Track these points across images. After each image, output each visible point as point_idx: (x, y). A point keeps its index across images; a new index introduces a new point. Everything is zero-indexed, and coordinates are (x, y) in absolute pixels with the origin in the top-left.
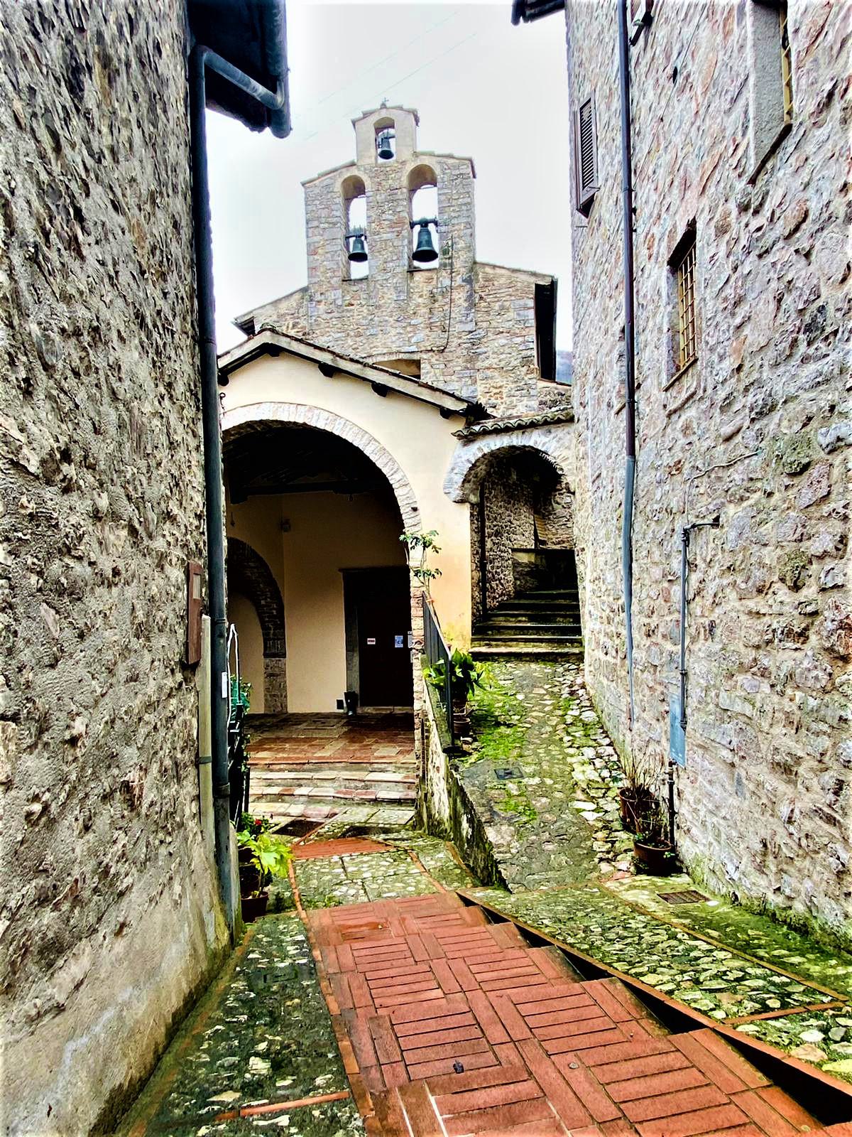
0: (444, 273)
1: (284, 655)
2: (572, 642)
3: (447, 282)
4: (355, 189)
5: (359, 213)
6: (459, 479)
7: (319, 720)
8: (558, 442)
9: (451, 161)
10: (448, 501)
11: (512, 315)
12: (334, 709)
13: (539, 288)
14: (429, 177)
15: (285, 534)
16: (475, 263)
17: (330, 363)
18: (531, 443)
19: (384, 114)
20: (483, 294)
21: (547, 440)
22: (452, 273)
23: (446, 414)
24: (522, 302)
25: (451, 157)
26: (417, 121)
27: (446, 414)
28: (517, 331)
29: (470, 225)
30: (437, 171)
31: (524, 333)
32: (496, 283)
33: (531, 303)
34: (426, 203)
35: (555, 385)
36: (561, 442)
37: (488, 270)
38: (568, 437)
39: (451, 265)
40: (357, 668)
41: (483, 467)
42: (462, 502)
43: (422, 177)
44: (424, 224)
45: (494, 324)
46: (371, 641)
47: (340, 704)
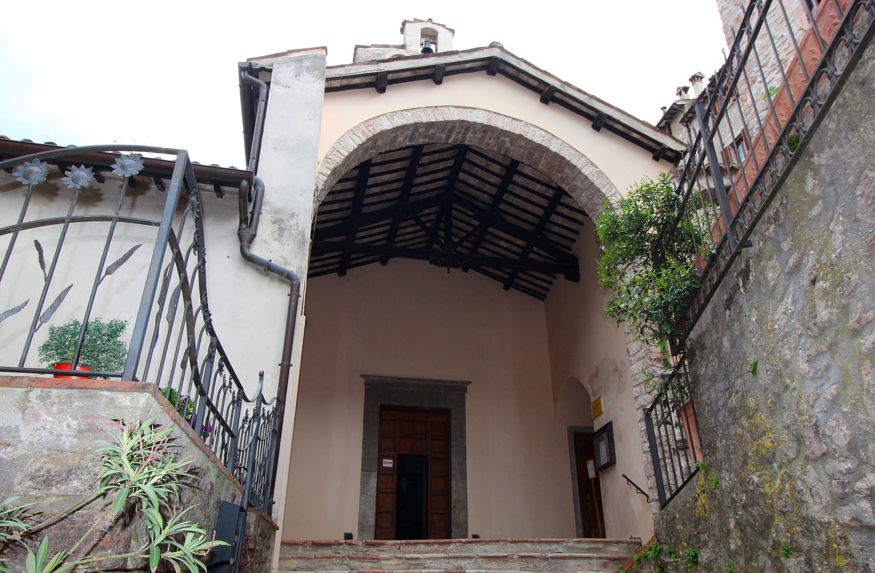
46: (388, 463)
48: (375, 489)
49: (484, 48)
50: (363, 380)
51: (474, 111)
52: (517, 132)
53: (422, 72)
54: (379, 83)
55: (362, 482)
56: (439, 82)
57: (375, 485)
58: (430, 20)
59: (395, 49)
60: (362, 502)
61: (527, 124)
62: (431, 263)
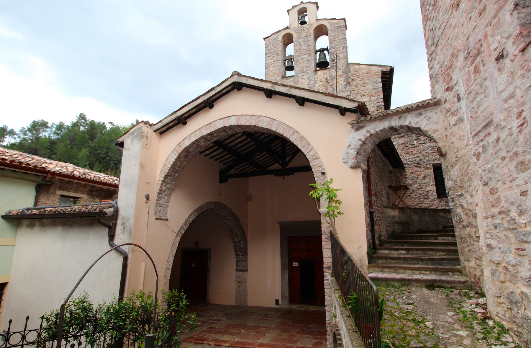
0: (333, 70)
1: (247, 271)
2: (453, 271)
3: (335, 74)
4: (288, 39)
5: (290, 50)
6: (353, 153)
7: (264, 313)
8: (428, 120)
9: (334, 21)
10: (347, 168)
11: (369, 86)
12: (274, 305)
13: (384, 73)
14: (324, 30)
15: (249, 203)
16: (348, 64)
17: (270, 88)
18: (407, 123)
19: (302, 6)
20: (353, 78)
22: (336, 70)
23: (343, 111)
24: (375, 80)
26: (318, 7)
27: (343, 111)
28: (373, 94)
29: (346, 48)
30: (328, 26)
31: (377, 94)
32: (360, 72)
33: (380, 80)
34: (323, 42)
36: (431, 120)
37: (356, 66)
38: (436, 116)
39: (336, 66)
40: (287, 280)
41: (370, 145)
42: (355, 167)
43: (320, 31)
44: (322, 51)
45: (360, 91)
46: (295, 264)
47: (277, 302)
48: (287, 279)
49: (228, 78)
50: (279, 225)
51: (231, 118)
52: (253, 124)
53: (201, 106)
54: (181, 120)
55: (282, 275)
56: (185, 123)
57: (287, 277)
58: (302, 2)
59: (283, 31)
60: (282, 285)
61: (259, 117)
62: (275, 175)
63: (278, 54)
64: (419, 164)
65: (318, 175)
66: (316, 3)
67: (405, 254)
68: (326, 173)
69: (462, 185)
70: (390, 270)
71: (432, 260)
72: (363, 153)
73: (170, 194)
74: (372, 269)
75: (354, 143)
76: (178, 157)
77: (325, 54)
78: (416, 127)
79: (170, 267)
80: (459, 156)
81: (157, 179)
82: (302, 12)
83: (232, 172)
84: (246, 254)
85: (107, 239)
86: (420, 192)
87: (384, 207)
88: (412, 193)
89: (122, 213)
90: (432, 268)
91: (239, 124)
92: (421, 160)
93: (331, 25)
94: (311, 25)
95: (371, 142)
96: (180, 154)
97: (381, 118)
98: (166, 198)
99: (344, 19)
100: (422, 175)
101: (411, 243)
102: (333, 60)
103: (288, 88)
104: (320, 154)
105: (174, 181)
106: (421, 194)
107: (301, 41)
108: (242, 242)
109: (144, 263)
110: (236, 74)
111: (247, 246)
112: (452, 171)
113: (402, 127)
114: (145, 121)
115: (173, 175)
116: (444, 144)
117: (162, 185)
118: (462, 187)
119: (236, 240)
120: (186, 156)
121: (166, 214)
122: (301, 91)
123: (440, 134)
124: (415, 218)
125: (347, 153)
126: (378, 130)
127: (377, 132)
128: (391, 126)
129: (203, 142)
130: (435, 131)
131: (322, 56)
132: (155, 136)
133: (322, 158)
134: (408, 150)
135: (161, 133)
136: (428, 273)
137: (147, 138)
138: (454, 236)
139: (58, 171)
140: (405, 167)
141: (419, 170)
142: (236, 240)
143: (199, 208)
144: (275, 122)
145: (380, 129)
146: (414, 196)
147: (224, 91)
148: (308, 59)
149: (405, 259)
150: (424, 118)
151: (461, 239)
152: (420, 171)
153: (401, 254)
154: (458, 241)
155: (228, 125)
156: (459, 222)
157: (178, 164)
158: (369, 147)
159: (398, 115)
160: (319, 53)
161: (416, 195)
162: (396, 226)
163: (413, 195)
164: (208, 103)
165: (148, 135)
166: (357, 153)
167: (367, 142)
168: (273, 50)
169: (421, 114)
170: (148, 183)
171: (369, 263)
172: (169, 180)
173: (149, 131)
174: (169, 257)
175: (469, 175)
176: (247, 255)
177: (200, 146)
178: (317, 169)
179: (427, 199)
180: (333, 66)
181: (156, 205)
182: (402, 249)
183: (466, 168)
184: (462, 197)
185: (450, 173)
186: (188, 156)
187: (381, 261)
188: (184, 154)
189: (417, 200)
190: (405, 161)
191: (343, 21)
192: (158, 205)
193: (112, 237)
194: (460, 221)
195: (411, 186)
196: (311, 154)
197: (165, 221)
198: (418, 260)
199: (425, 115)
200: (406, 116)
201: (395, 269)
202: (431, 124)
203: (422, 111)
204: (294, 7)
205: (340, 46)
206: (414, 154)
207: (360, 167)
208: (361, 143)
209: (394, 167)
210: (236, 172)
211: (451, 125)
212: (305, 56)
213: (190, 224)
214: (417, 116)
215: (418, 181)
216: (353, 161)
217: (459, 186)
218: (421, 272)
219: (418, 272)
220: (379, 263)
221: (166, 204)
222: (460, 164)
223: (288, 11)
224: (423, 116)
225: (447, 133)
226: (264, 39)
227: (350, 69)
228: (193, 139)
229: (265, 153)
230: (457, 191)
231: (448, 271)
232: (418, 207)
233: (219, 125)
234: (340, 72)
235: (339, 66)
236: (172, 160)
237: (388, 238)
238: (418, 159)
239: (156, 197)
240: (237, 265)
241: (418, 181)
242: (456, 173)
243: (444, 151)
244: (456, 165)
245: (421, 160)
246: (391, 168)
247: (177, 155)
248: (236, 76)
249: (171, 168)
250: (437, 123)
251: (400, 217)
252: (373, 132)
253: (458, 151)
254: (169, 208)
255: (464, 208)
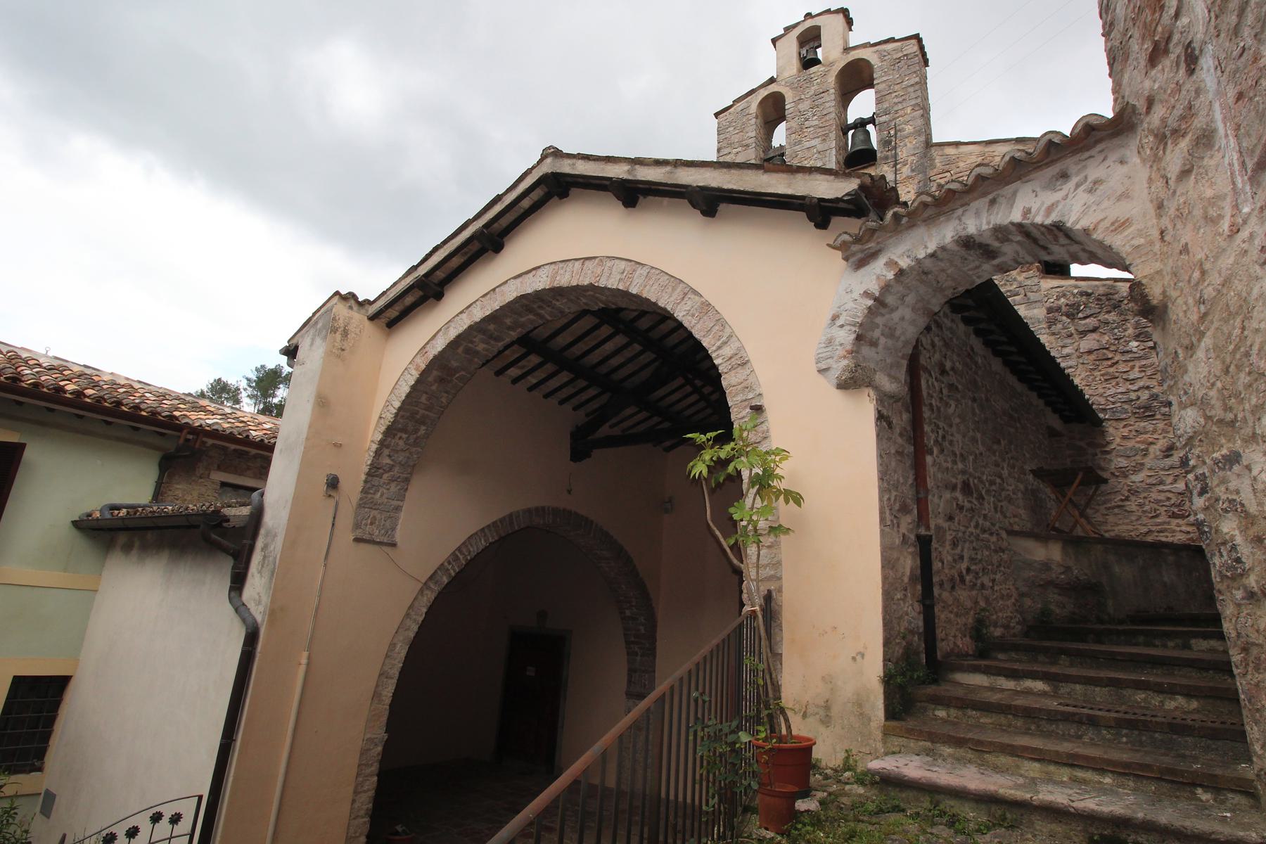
2: (1217, 786)
6: (845, 337)
8: (1090, 191)
10: (827, 387)
17: (625, 176)
18: (1016, 216)
19: (810, 23)
21: (1058, 196)
22: (895, 166)
25: (892, 40)
26: (850, 22)
32: (961, 164)
35: (1072, 282)
37: (950, 151)
38: (1123, 170)
42: (849, 384)
43: (856, 77)
44: (861, 124)
49: (533, 168)
58: (808, 16)
63: (747, 146)
64: (1147, 408)
65: (744, 413)
66: (844, 12)
67: (1044, 694)
68: (766, 406)
69: (1230, 416)
70: (961, 752)
71: (1134, 725)
72: (883, 340)
73: (407, 480)
74: (897, 741)
75: (850, 305)
76: (418, 381)
77: (868, 133)
78: (1048, 222)
79: (395, 672)
80: (1209, 292)
81: (369, 438)
82: (810, 38)
83: (604, 431)
84: (651, 652)
85: (227, 583)
86: (1154, 496)
87: (1011, 533)
88: (1127, 499)
89: (269, 519)
90: (1127, 765)
91: (556, 284)
92: (1154, 397)
93: (882, 58)
94: (832, 64)
95: (910, 299)
96: (424, 374)
97: (929, 212)
98: (394, 488)
99: (917, 37)
100: (1162, 443)
101: (1080, 654)
102: (886, 143)
103: (668, 168)
104: (751, 352)
105: (416, 444)
106: (1157, 502)
107: (804, 106)
108: (642, 619)
109: (305, 654)
110: (553, 153)
111: (655, 631)
112: (1191, 368)
113: (1001, 232)
114: (343, 292)
115: (410, 428)
116: (1158, 266)
117: (378, 453)
118: (1232, 423)
119: (628, 613)
120: (441, 380)
121: (393, 529)
122: (702, 170)
123: (1140, 233)
124: (1124, 571)
125: (830, 342)
126: (921, 255)
127: (919, 261)
128: (963, 234)
129: (483, 341)
130: (1120, 225)
131: (861, 137)
132: (367, 332)
133: (756, 364)
134: (1111, 370)
135: (392, 324)
136: (1108, 780)
137: (345, 333)
138: (1221, 636)
139: (209, 425)
140: (1102, 421)
141: (1150, 428)
142: (628, 613)
143: (502, 520)
144: (640, 271)
145: (930, 251)
146: (1134, 508)
147: (526, 203)
148: (820, 147)
149: (1029, 714)
150: (1078, 186)
151: (1245, 650)
152: (1154, 431)
153: (1028, 692)
154: (1236, 657)
155: (529, 291)
156: (1233, 578)
157: (424, 399)
158: (906, 321)
159: (984, 195)
160: (851, 132)
161: (1140, 505)
162: (1053, 596)
163: (1132, 505)
164: (487, 238)
165: (351, 328)
166: (859, 338)
167: (890, 300)
168: (736, 139)
169: (1064, 176)
170: (338, 446)
171: (891, 714)
172: (401, 443)
173: (358, 319)
174: (392, 646)
175: (1254, 358)
176: (655, 657)
177: (477, 352)
178: (739, 398)
179: (1183, 517)
180: (886, 158)
181: (362, 504)
182: (1034, 676)
183: (1237, 331)
184: (1236, 468)
185: (1187, 378)
186: (442, 376)
187: (941, 713)
188: (435, 373)
189: (1145, 520)
190: (1102, 401)
191: (914, 41)
192: (366, 501)
193: (238, 581)
194: (1237, 571)
195: (1126, 477)
196: (727, 351)
197: (385, 548)
198: (1080, 722)
199: (1081, 177)
200: (1015, 194)
201: (979, 749)
202: (1106, 204)
203: (1070, 163)
204: (788, 29)
205: (904, 105)
206: (1132, 381)
207: (870, 384)
208: (870, 302)
209: (1066, 420)
210: (616, 431)
211: (1172, 176)
212: (813, 143)
213: (468, 563)
214: (1051, 186)
215: (1148, 461)
216: (845, 362)
217: (1221, 421)
218: (1080, 774)
219: (1064, 774)
220: (936, 718)
221: (396, 503)
222: (1216, 324)
223: (774, 41)
224: (1074, 180)
225: (1165, 222)
226: (717, 115)
227: (932, 160)
228: (453, 333)
229: (679, 381)
230: (1214, 444)
231: (1195, 785)
232: (1149, 539)
233: (511, 293)
234: (906, 171)
235: (903, 154)
236: (405, 389)
237: (1026, 634)
238: (1145, 395)
239: (362, 484)
240: (629, 682)
241: (1148, 461)
242: (1204, 370)
243: (1155, 293)
244: (1202, 334)
245: (1154, 397)
246: (1054, 421)
247: (416, 374)
248: (549, 160)
249: (400, 409)
250: (1125, 196)
251: (1068, 569)
252: (904, 263)
253: (1203, 273)
254: (402, 515)
255: (1247, 514)
